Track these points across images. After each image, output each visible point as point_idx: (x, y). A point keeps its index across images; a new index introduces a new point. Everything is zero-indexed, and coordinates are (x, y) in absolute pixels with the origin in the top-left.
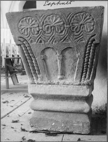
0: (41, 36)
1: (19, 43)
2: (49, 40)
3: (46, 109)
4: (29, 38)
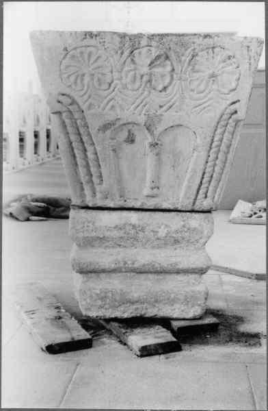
0: (116, 95)
1: (58, 107)
2: (133, 106)
3: (145, 330)
4: (86, 97)
